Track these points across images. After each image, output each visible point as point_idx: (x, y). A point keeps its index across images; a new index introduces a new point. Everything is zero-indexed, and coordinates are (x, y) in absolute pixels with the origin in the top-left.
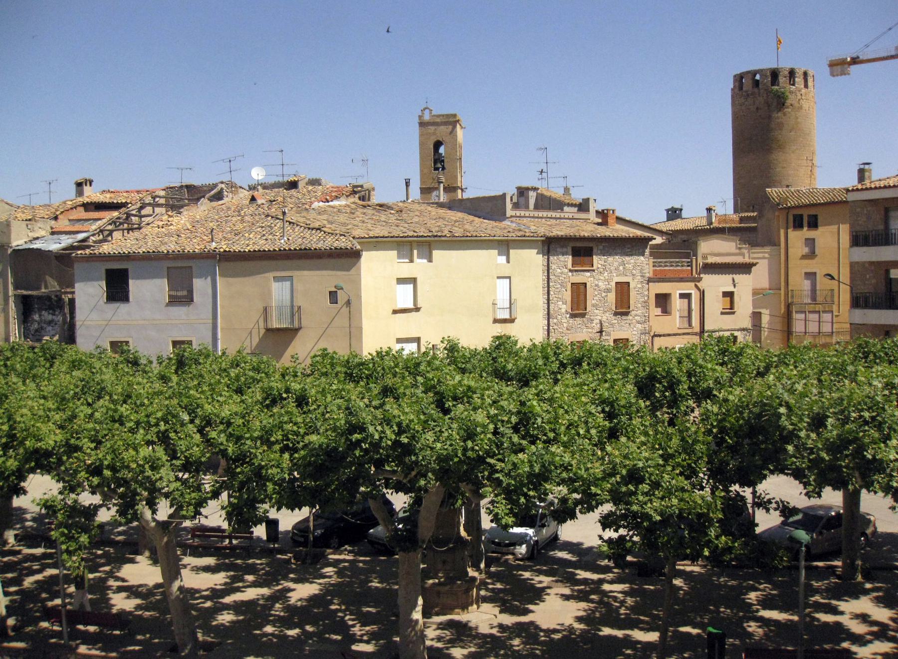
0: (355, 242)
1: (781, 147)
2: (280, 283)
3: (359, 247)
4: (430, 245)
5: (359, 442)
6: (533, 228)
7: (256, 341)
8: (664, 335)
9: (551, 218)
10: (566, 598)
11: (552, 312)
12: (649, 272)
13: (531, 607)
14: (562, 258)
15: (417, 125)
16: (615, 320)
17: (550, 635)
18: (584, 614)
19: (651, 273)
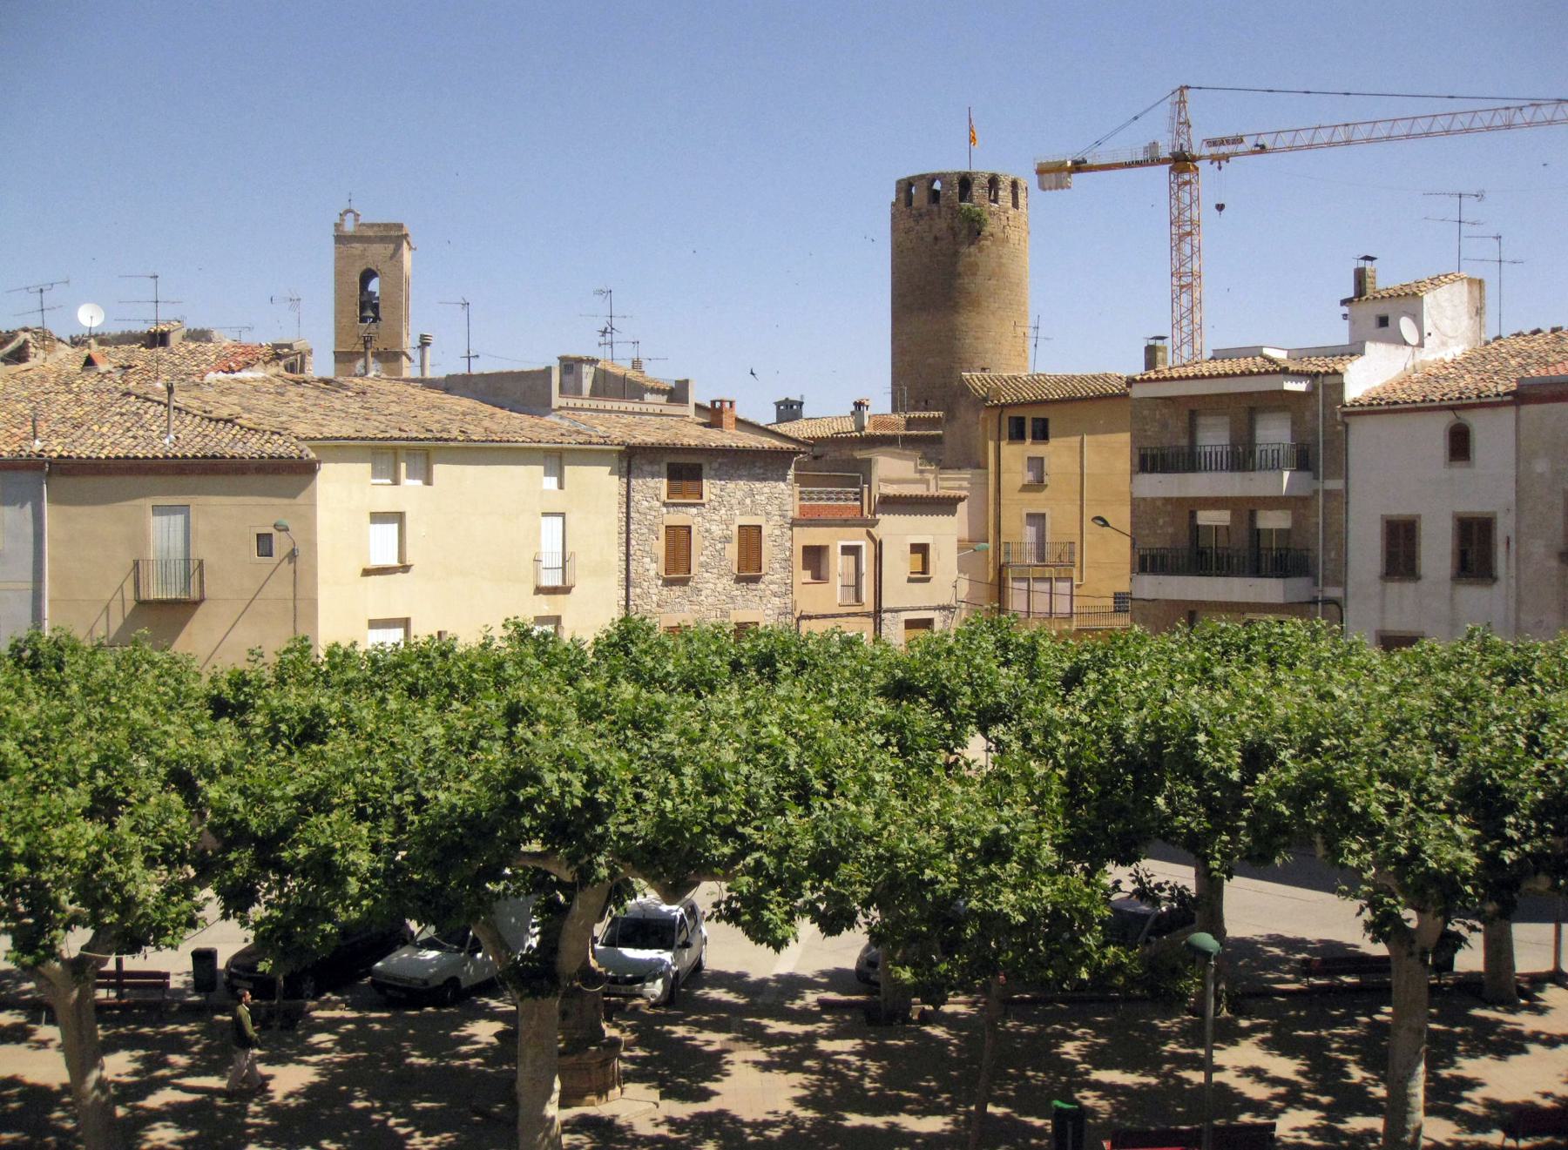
0: (303, 445)
1: (975, 303)
2: (165, 518)
3: (313, 455)
4: (427, 454)
5: (531, 800)
6: (601, 430)
7: (117, 622)
8: (817, 617)
9: (625, 412)
10: (766, 1067)
11: (632, 575)
12: (793, 510)
13: (711, 1086)
14: (651, 482)
15: (332, 240)
16: (737, 590)
17: (761, 1131)
18: (806, 1092)
19: (797, 509)
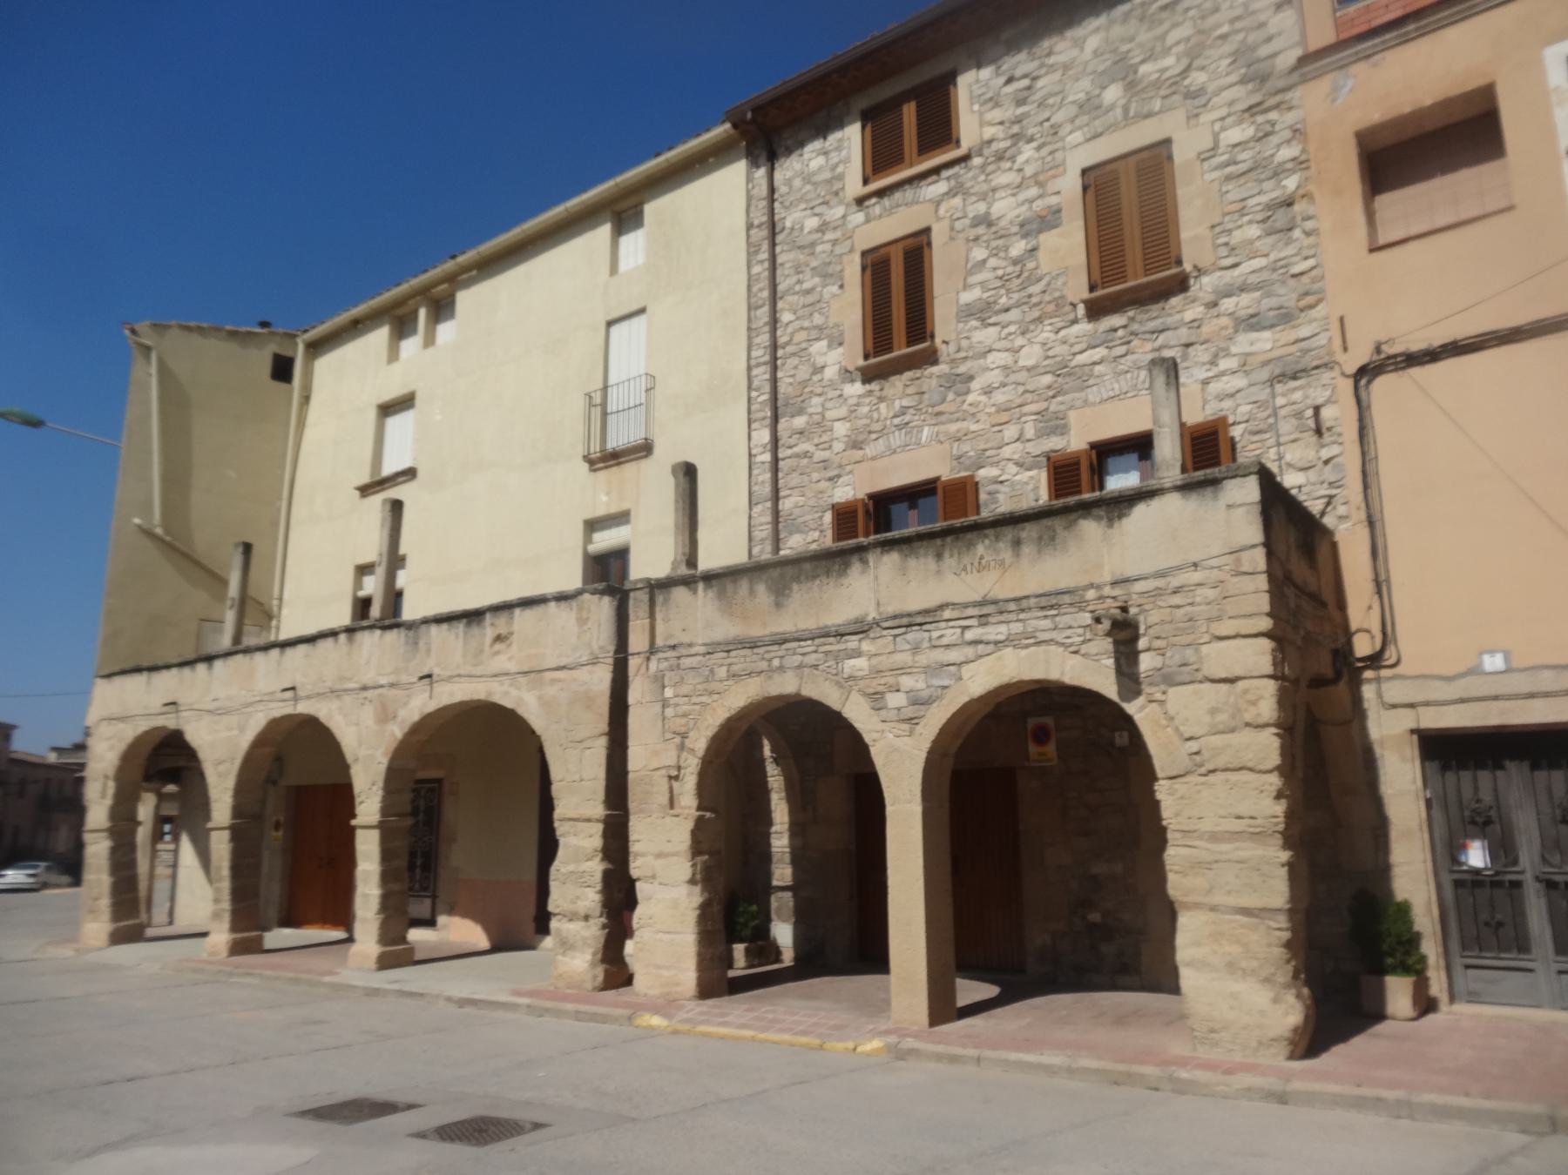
11: (783, 388)
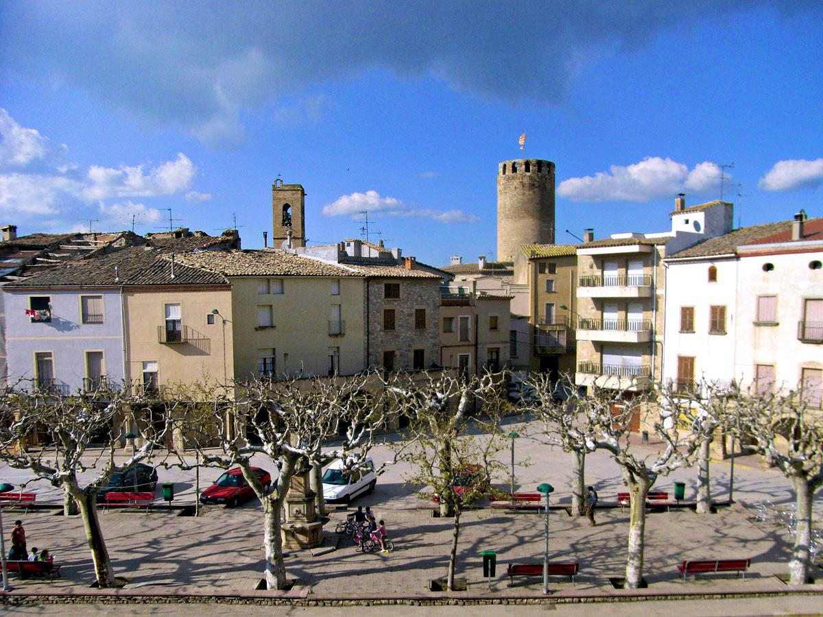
11: (370, 329)
